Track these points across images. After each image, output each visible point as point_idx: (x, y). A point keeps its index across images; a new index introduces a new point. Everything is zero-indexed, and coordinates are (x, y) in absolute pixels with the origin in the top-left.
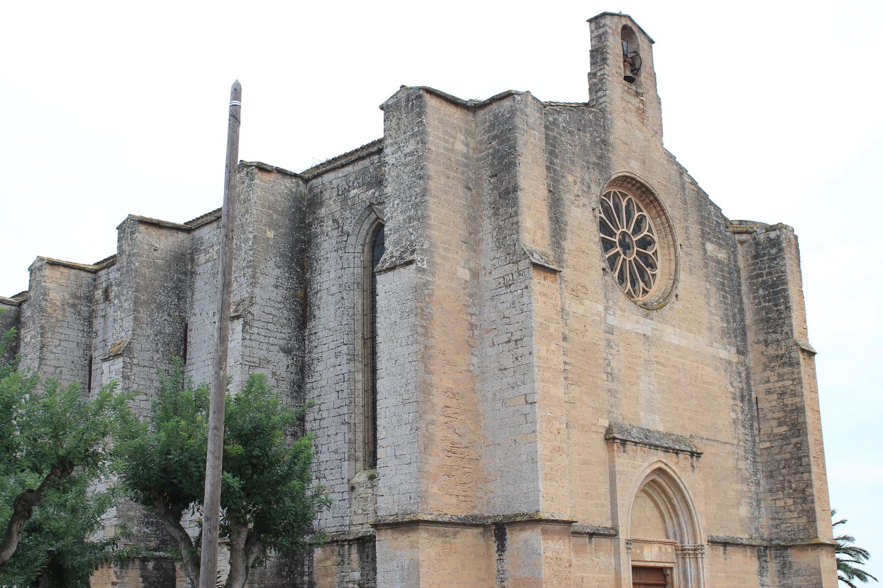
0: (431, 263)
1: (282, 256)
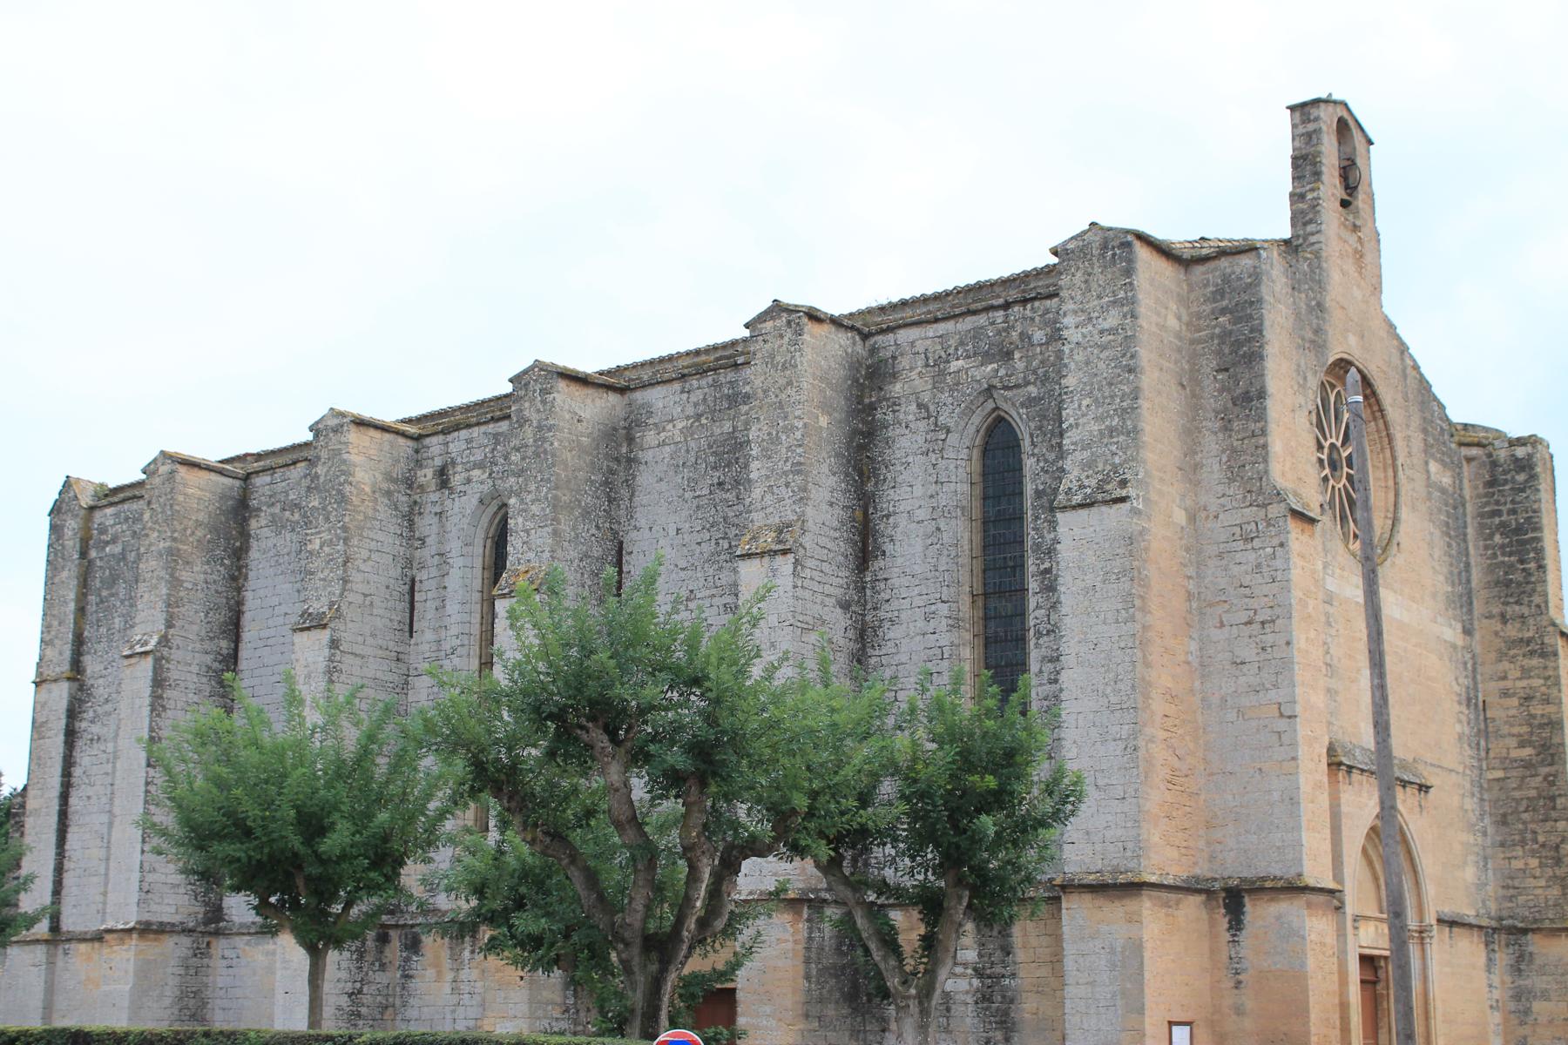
0: (1147, 500)
1: (837, 455)
